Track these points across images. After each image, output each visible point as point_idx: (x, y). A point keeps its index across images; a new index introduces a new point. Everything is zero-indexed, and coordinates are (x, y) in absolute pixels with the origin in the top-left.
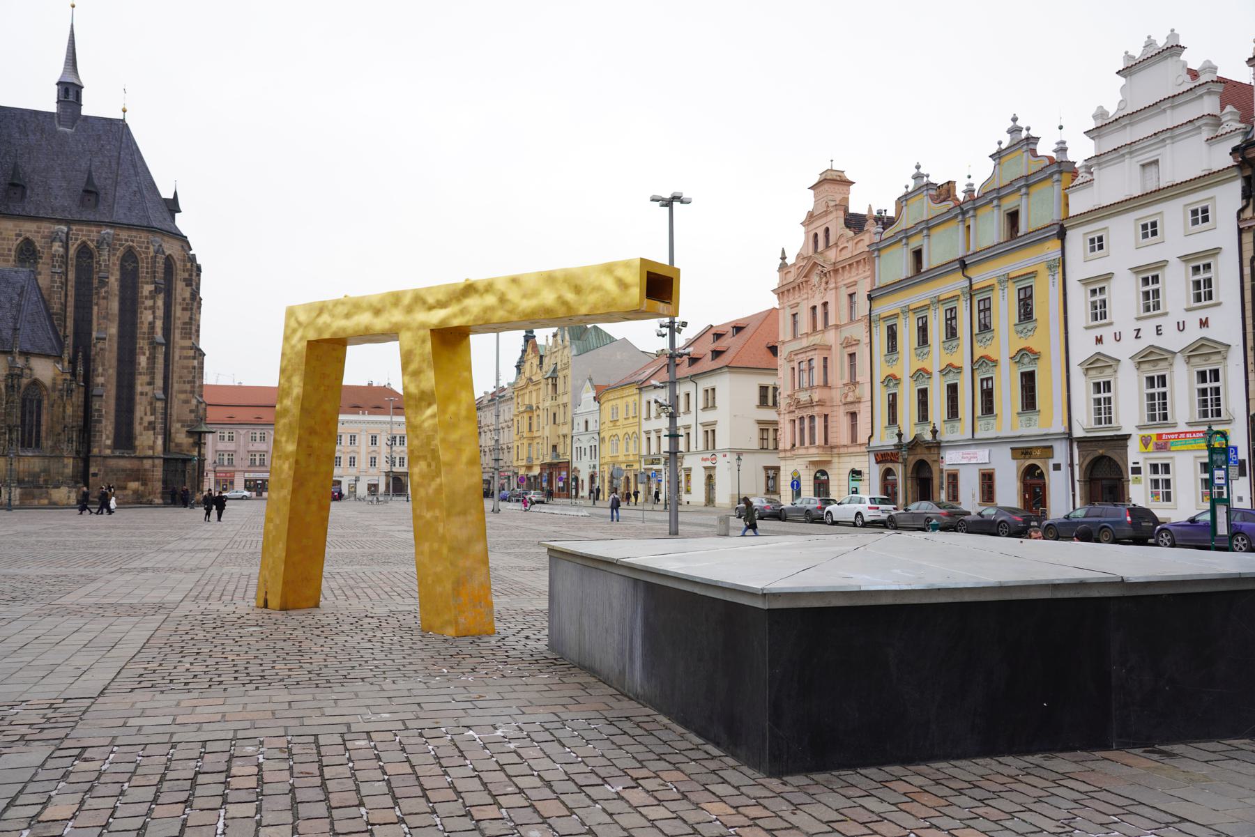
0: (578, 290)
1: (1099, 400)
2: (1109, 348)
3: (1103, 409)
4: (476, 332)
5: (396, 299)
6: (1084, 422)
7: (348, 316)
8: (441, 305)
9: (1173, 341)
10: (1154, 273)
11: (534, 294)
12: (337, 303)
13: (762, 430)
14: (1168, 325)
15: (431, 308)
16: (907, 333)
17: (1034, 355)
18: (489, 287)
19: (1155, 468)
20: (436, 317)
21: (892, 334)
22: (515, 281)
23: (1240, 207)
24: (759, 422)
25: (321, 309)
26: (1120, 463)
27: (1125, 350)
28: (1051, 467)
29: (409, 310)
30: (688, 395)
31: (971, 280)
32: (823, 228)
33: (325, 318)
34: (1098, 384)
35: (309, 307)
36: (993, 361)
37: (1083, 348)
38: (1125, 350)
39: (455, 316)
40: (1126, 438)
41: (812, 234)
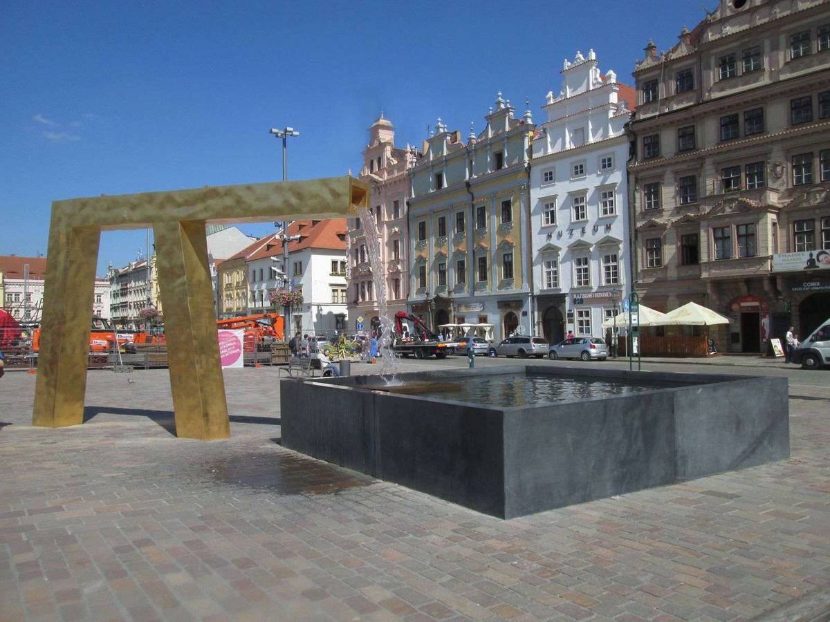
0: (299, 195)
1: (550, 272)
2: (554, 241)
3: (554, 278)
4: (118, 223)
5: (150, 198)
6: (541, 284)
7: (109, 209)
8: (187, 203)
9: (591, 238)
10: (606, 215)
11: (266, 198)
12: (97, 200)
13: (334, 291)
14: (589, 228)
15: (179, 206)
16: (433, 226)
17: (510, 246)
18: (228, 192)
19: (581, 314)
20: (182, 213)
21: (422, 227)
22: (249, 188)
23: (628, 159)
24: (331, 285)
25: (84, 204)
26: (562, 312)
27: (563, 244)
28: (521, 314)
29: (162, 206)
30: (255, 272)
31: (473, 195)
32: (377, 157)
33: (87, 211)
34: (606, 194)
35: (73, 202)
36: (822, 119)
37: (539, 242)
38: (563, 244)
39: (201, 211)
40: (564, 295)
41: (369, 160)
